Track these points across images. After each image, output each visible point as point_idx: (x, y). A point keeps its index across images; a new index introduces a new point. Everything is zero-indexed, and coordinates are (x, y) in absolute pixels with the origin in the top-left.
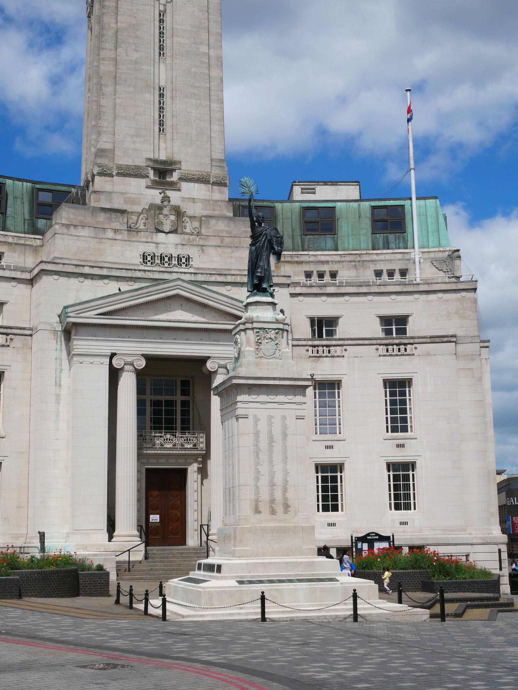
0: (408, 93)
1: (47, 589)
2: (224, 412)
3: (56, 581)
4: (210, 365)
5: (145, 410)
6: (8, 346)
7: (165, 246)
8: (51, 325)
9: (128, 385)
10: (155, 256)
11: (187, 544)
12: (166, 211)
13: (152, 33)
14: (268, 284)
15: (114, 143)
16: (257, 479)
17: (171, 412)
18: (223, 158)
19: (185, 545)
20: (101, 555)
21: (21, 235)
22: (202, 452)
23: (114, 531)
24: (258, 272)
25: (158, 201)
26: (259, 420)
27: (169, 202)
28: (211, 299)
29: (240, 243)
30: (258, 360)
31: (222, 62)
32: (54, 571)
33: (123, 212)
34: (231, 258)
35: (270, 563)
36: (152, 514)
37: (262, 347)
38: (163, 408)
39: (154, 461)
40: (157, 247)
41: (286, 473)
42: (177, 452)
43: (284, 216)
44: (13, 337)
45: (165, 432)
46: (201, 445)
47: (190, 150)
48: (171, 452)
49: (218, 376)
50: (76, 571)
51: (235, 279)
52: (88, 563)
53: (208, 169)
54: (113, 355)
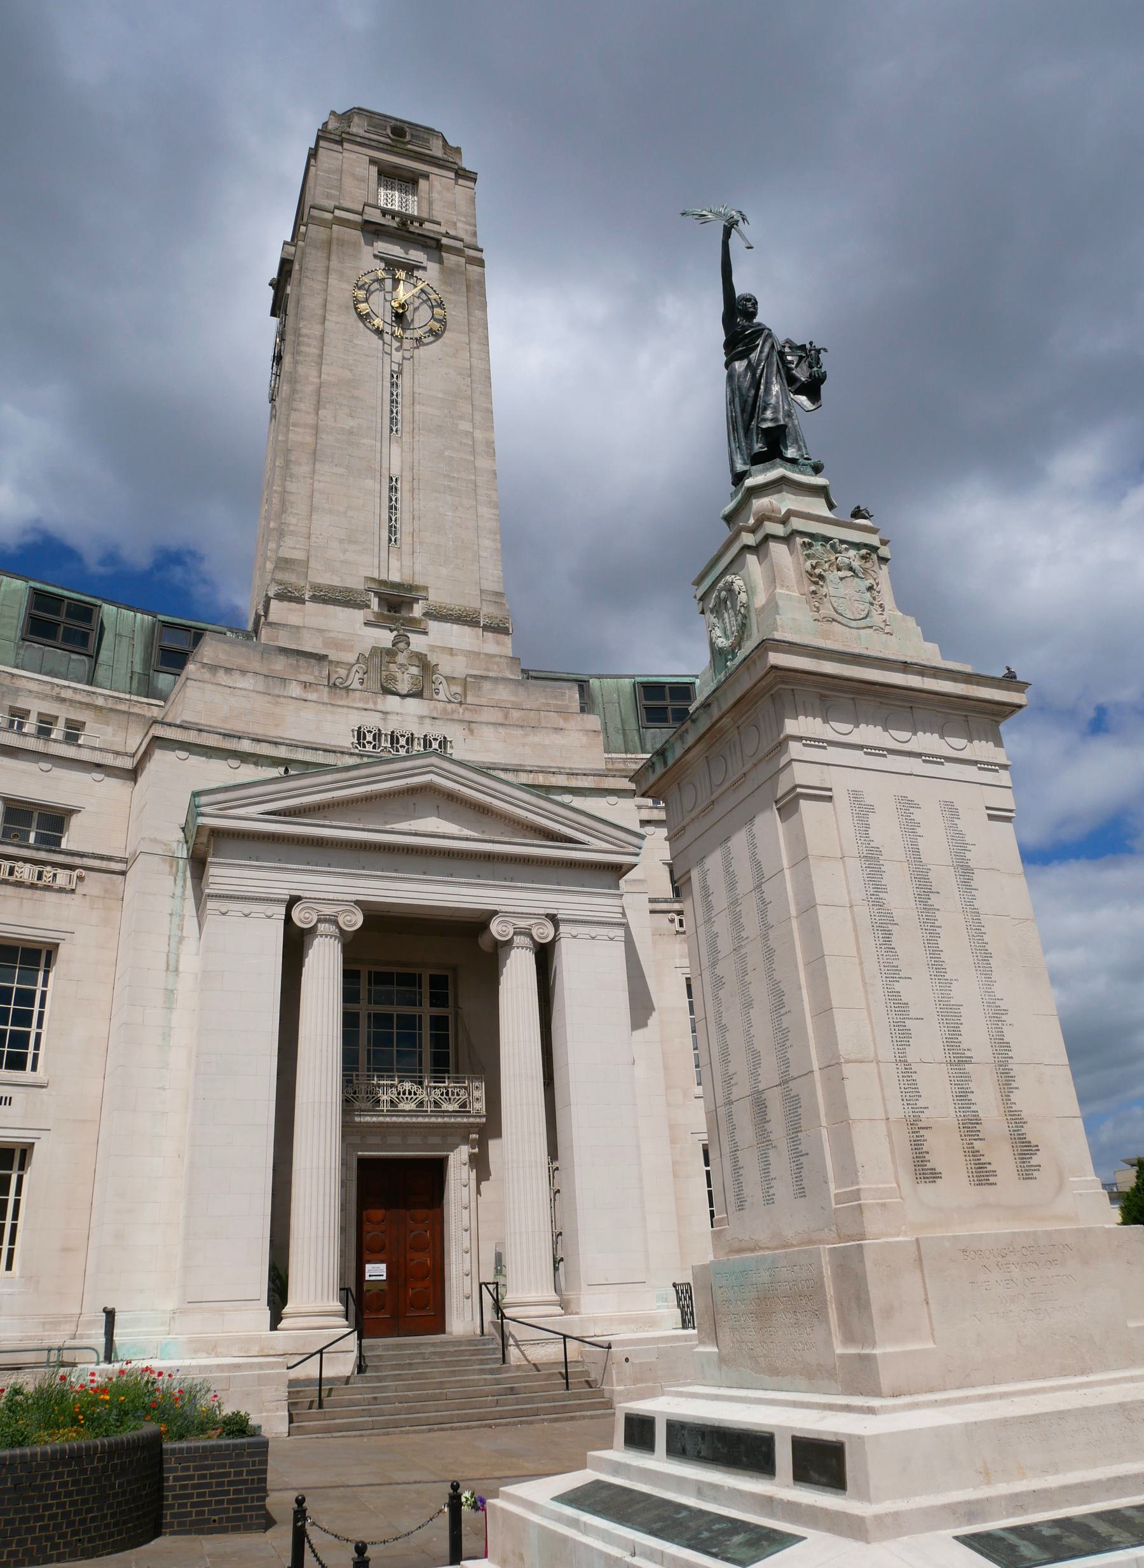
1: (30, 1530)
3: (68, 1494)
4: (497, 928)
6: (73, 891)
7: (400, 718)
8: (165, 845)
9: (324, 965)
11: (447, 1329)
12: (401, 658)
13: (380, 395)
14: (799, 449)
15: (308, 551)
16: (902, 1036)
17: (411, 1040)
19: (443, 1331)
20: (251, 1366)
21: (122, 695)
22: (478, 1120)
23: (284, 1301)
24: (765, 420)
27: (408, 644)
30: (826, 626)
32: (63, 1451)
33: (321, 658)
34: (524, 745)
35: (1061, 1415)
36: (369, 1262)
37: (827, 589)
38: (395, 1031)
39: (376, 1140)
41: (997, 1015)
42: (427, 1120)
44: (84, 873)
45: (399, 1077)
46: (477, 1106)
47: (444, 571)
48: (414, 1120)
49: (513, 952)
50: (152, 1447)
52: (204, 1403)
54: (293, 901)
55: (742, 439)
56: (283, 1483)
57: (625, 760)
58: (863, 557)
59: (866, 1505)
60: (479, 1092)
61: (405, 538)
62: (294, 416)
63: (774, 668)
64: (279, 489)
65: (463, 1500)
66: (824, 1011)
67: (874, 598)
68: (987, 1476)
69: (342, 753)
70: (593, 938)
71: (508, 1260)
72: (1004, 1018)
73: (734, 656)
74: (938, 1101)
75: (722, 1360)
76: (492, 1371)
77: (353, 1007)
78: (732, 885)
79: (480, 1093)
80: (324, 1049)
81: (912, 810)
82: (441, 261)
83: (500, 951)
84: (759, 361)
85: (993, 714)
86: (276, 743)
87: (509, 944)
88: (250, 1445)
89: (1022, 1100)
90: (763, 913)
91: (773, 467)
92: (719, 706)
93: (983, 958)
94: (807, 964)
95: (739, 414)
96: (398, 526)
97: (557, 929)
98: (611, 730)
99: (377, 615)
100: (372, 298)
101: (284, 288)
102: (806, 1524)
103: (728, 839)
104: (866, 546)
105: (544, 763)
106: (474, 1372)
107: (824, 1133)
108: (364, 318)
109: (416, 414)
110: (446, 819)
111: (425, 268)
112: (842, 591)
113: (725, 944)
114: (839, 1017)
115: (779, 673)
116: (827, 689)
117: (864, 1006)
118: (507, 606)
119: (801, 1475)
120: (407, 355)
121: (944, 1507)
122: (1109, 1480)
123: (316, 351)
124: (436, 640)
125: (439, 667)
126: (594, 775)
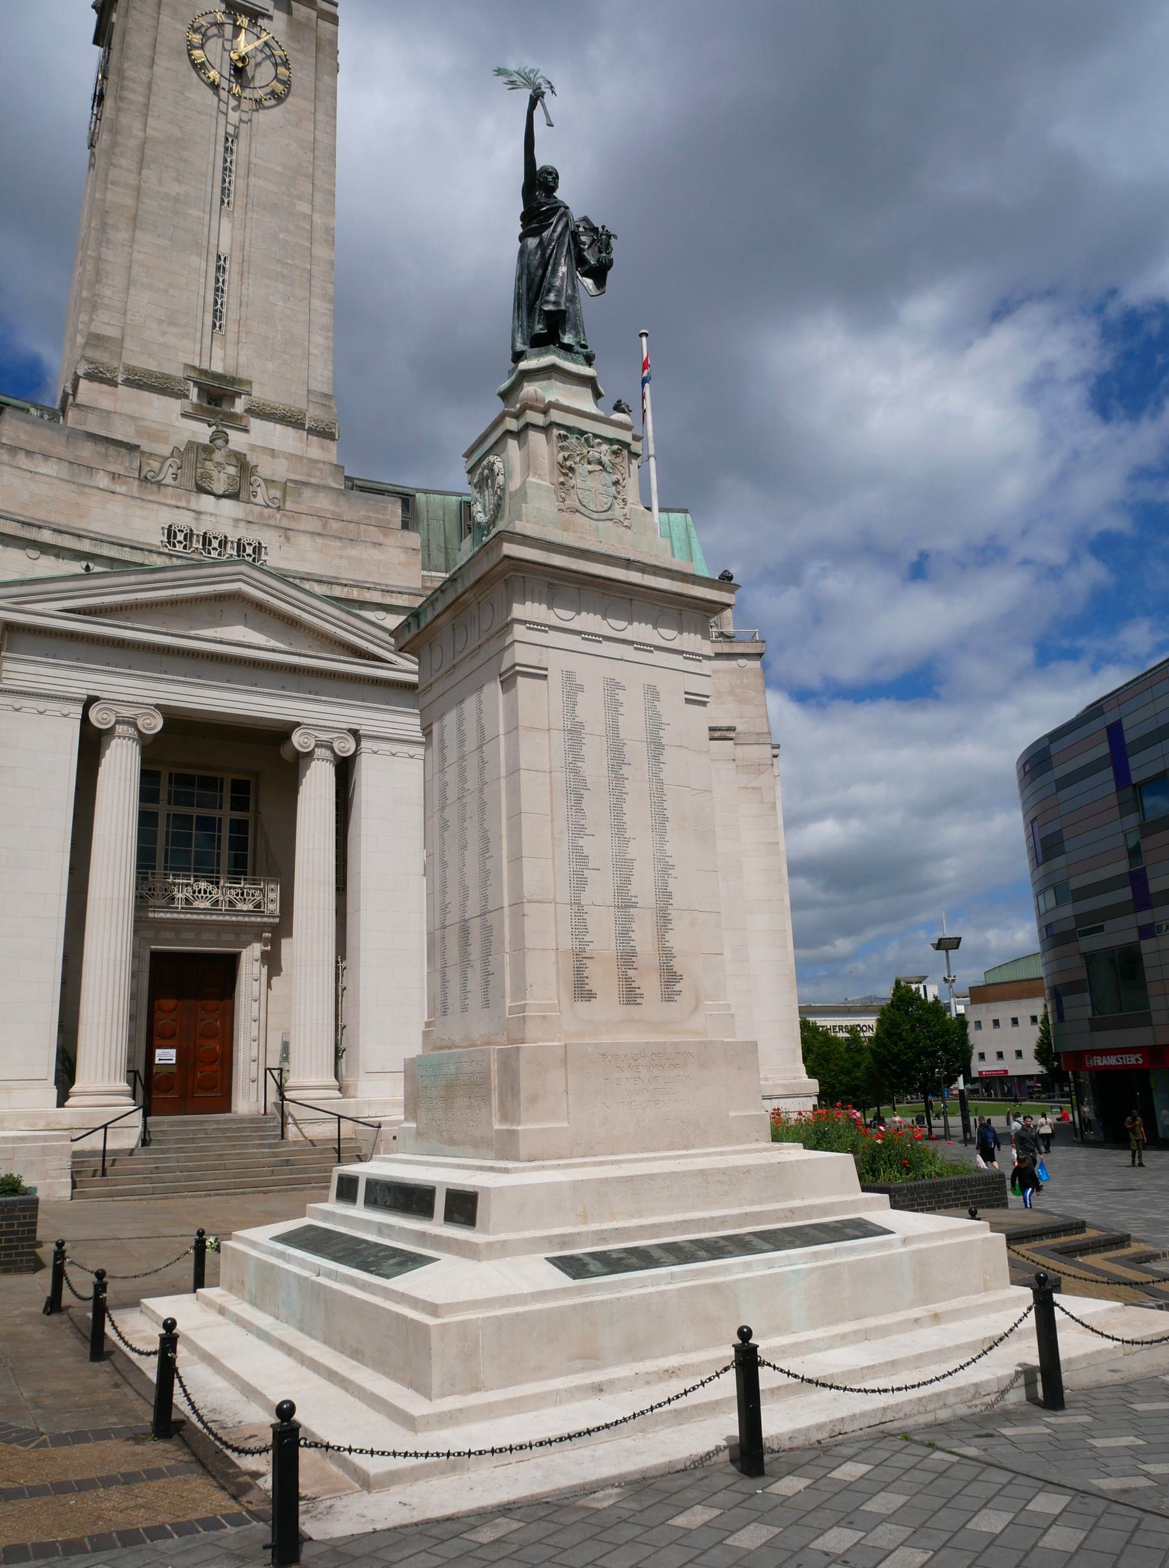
5: (156, 833)
9: (121, 768)
10: (192, 535)
12: (218, 456)
14: (576, 336)
15: (123, 329)
16: (579, 882)
18: (329, 392)
19: (229, 1111)
20: (35, 1138)
22: (271, 920)
23: (72, 1081)
24: (548, 302)
25: (206, 440)
26: (581, 688)
27: (227, 442)
28: (307, 608)
29: (359, 533)
30: (567, 516)
33: (133, 448)
34: (341, 557)
35: (652, 1177)
36: (160, 1047)
37: (576, 481)
40: (197, 519)
41: (665, 868)
42: (221, 918)
46: (272, 907)
47: (270, 366)
48: (208, 917)
49: (313, 764)
53: (301, 404)
54: (90, 701)
55: (525, 319)
56: (47, 1232)
58: (614, 453)
59: (486, 1236)
60: (274, 894)
61: (231, 327)
62: (114, 174)
63: (507, 557)
64: (93, 254)
65: (208, 1244)
66: (517, 859)
67: (618, 493)
68: (585, 1218)
69: (150, 551)
70: (394, 755)
71: (292, 1048)
72: (670, 872)
73: (489, 533)
74: (603, 937)
75: (419, 1134)
76: (270, 1146)
77: (151, 807)
78: (462, 742)
79: (275, 895)
80: (118, 848)
82: (289, 11)
83: (301, 761)
84: (550, 239)
86: (79, 536)
87: (309, 755)
88: (21, 1202)
89: (674, 940)
90: (482, 769)
91: (547, 353)
92: (463, 584)
93: (661, 820)
94: (509, 818)
96: (224, 311)
97: (358, 744)
98: (433, 547)
99: (195, 406)
100: (209, 45)
101: (109, 15)
102: (444, 1251)
103: (462, 701)
104: (619, 442)
105: (360, 577)
106: (253, 1146)
107: (507, 957)
108: (199, 68)
109: (251, 188)
110: (253, 629)
111: (270, 18)
112: (590, 484)
113: (452, 793)
114: (527, 864)
115: (512, 562)
117: (550, 856)
118: (335, 410)
119: (449, 1218)
120: (245, 117)
121: (543, 1238)
122: (676, 1222)
123: (141, 99)
124: (260, 438)
125: (258, 469)
126: (409, 594)
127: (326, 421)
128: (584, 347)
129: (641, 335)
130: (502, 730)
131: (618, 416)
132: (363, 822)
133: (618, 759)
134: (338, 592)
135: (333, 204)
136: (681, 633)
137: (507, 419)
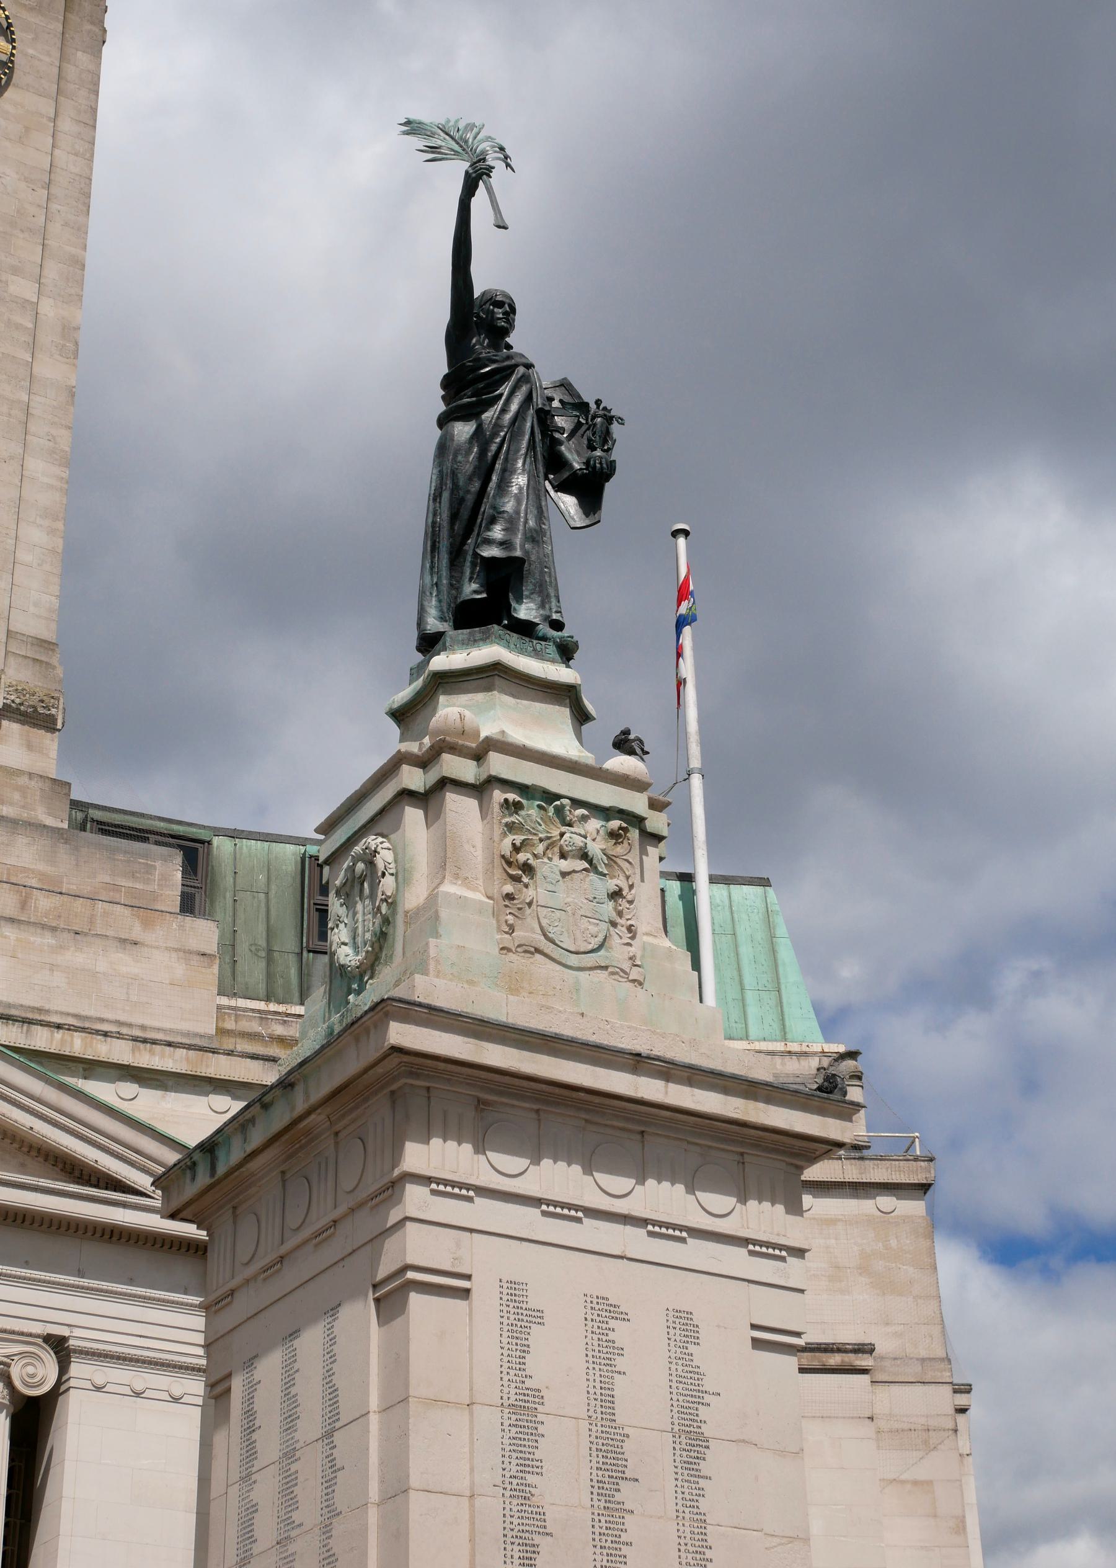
0: (681, 541)
2: (228, 1318)
14: (542, 606)
18: (50, 636)
24: (489, 542)
29: (92, 920)
30: (517, 960)
31: (77, 344)
34: (53, 967)
43: (239, 880)
51: (63, 1041)
55: (444, 573)
57: (263, 1016)
58: (613, 835)
67: (620, 914)
78: (290, 1421)
81: (612, 1323)
84: (497, 426)
85: (793, 1155)
90: (330, 1484)
91: (486, 639)
95: (445, 524)
97: (63, 1368)
98: (243, 948)
103: (294, 1334)
104: (622, 814)
112: (564, 897)
115: (406, 1058)
116: (492, 1091)
118: (60, 672)
126: (189, 1047)
127: (41, 694)
128: (558, 625)
129: (675, 534)
130: (374, 1402)
131: (621, 763)
132: (63, 1544)
133: (611, 1469)
134: (41, 1040)
135: (81, 283)
136: (743, 1200)
137: (405, 768)
